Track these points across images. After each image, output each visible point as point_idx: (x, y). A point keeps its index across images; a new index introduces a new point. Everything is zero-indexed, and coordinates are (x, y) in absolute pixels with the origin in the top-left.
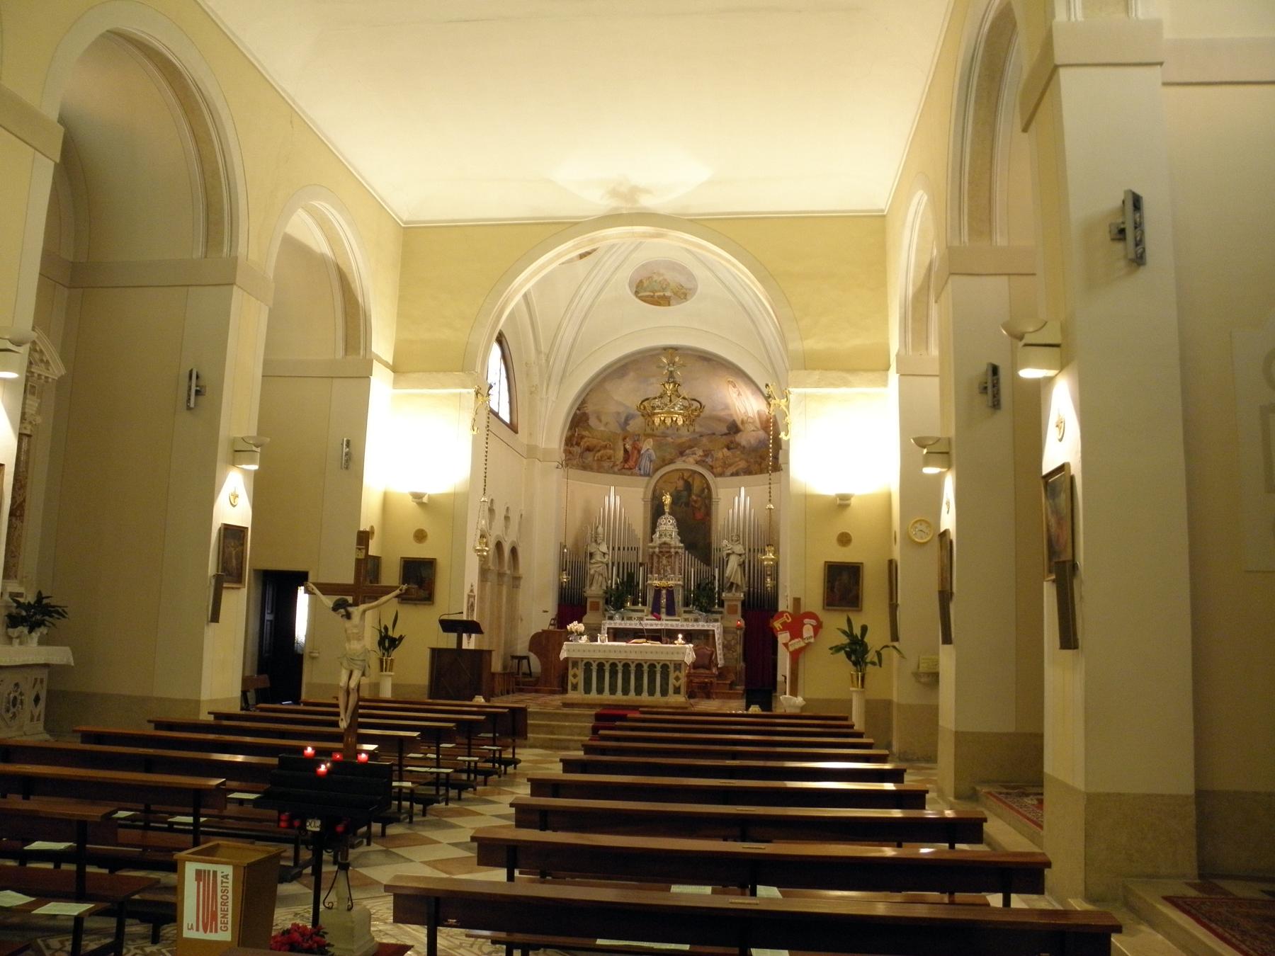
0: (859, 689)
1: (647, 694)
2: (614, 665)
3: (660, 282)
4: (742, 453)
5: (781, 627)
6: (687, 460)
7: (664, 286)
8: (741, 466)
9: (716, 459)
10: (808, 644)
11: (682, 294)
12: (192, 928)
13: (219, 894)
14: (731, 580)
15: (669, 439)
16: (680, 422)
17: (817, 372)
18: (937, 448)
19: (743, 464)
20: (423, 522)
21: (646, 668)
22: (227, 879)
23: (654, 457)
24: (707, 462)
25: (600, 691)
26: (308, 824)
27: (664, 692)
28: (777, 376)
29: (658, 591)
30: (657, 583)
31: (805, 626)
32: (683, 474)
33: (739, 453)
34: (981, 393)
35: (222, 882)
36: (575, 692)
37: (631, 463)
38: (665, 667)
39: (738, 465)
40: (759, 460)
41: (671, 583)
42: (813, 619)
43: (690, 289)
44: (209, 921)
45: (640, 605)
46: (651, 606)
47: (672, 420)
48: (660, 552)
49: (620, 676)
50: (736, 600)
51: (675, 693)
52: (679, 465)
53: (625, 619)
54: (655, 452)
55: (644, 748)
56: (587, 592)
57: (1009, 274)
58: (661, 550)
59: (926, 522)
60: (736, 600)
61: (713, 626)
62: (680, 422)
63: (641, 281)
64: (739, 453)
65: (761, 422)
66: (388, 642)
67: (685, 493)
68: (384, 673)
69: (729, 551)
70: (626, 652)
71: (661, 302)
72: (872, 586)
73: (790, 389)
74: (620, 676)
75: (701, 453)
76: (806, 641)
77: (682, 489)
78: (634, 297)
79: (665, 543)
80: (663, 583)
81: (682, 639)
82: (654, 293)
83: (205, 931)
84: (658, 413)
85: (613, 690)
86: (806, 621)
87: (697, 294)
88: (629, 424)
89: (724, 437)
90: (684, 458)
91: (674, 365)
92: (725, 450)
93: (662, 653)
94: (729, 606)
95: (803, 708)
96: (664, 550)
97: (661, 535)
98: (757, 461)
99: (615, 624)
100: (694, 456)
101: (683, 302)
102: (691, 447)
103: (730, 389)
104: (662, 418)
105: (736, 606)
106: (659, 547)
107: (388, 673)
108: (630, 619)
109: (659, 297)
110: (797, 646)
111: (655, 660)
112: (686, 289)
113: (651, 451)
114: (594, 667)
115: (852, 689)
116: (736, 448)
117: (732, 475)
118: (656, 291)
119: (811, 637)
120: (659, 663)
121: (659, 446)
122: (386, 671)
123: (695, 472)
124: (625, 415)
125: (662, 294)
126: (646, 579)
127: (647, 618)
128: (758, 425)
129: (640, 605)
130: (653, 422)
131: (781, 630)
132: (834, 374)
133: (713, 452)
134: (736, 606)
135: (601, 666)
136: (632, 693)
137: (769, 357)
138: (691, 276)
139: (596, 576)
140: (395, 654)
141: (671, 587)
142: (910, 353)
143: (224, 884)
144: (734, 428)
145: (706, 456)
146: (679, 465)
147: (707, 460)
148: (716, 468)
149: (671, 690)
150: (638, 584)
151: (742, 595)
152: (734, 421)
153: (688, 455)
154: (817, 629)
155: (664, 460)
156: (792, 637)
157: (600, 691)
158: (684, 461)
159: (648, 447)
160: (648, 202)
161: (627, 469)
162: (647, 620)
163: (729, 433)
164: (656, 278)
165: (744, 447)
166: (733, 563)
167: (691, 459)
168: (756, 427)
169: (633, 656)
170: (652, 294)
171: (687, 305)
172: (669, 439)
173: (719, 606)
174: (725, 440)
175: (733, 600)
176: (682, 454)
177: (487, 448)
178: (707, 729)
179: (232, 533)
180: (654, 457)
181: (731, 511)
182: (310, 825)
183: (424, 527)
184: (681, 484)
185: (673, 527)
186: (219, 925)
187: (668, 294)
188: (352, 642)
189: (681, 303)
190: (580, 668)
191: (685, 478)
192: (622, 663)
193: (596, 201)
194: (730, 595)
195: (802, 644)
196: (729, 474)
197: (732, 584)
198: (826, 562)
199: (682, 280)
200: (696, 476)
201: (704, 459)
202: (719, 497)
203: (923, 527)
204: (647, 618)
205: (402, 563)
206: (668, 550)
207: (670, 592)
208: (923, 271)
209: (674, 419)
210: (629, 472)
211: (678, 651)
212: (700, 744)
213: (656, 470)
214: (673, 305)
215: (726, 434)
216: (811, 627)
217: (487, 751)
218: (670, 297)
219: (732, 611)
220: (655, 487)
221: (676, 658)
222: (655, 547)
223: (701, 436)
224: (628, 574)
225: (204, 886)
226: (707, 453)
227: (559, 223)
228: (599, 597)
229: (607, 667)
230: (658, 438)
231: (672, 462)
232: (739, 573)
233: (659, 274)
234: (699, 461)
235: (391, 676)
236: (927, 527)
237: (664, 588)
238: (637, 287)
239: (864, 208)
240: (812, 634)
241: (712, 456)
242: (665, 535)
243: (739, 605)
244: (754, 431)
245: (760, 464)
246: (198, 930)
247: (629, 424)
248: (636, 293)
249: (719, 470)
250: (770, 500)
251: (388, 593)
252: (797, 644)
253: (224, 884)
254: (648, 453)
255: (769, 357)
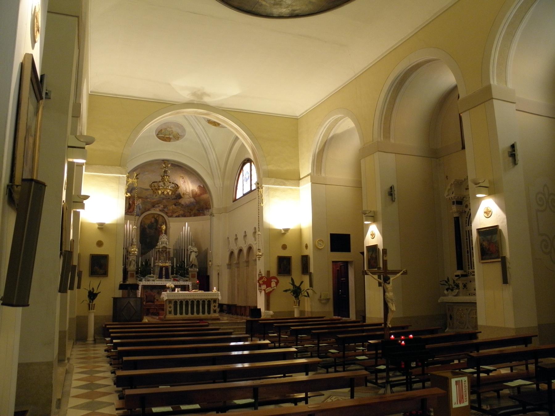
0: (298, 307)
1: (179, 314)
2: (204, 302)
3: (170, 131)
4: (181, 207)
5: (262, 283)
6: (156, 209)
7: (171, 133)
8: (181, 213)
9: (169, 210)
10: (273, 290)
11: (177, 137)
12: (456, 404)
13: (464, 388)
14: (193, 263)
15: (149, 200)
16: (170, 193)
17: (273, 179)
18: (370, 215)
19: (182, 212)
20: (100, 237)
21: (201, 302)
22: (466, 382)
23: (141, 207)
24: (165, 211)
25: (192, 313)
26: (412, 364)
27: (209, 312)
28: (213, 176)
29: (161, 268)
30: (161, 264)
31: (272, 283)
32: (154, 215)
33: (180, 207)
34: (389, 195)
35: (464, 383)
36: (171, 315)
37: (131, 210)
38: (209, 302)
39: (179, 213)
40: (190, 211)
41: (167, 264)
42: (275, 279)
43: (181, 136)
44: (461, 400)
45: (152, 274)
46: (158, 274)
47: (167, 192)
48: (162, 251)
49: (190, 306)
50: (195, 272)
51: (214, 313)
52: (152, 211)
53: (147, 281)
54: (142, 205)
55: (215, 338)
56: (129, 269)
57: (395, 153)
58: (163, 250)
59: (322, 241)
60: (195, 272)
61: (189, 283)
62: (170, 193)
63: (161, 130)
64: (180, 207)
65: (193, 195)
66: (92, 295)
67: (155, 224)
68: (91, 311)
69: (192, 251)
70: (193, 296)
71: (167, 140)
72: (296, 266)
73: (263, 185)
74: (190, 306)
75: (162, 206)
76: (273, 288)
77: (154, 222)
78: (156, 137)
79: (164, 247)
80: (164, 265)
81: (216, 289)
82: (165, 136)
83: (460, 404)
84: (161, 189)
85: (187, 313)
86: (273, 280)
87: (184, 138)
88: (132, 192)
89: (174, 200)
90: (154, 208)
91: (168, 168)
92: (174, 206)
93: (209, 295)
94: (192, 274)
95: (272, 316)
96: (164, 250)
97: (162, 243)
98: (189, 211)
99: (143, 283)
100: (159, 208)
101: (177, 141)
102: (158, 204)
103: (180, 179)
104: (163, 191)
105: (195, 274)
106: (162, 249)
107: (93, 311)
108: (149, 281)
109: (167, 138)
110: (269, 291)
111: (205, 299)
112: (180, 136)
113: (140, 205)
114: (178, 303)
115: (294, 307)
116: (179, 205)
117: (176, 217)
118: (166, 135)
119: (275, 287)
120: (201, 300)
121: (144, 203)
122: (91, 310)
123: (159, 215)
124: (131, 188)
125: (168, 136)
126: (154, 263)
127: (157, 280)
128: (191, 196)
129: (152, 274)
130: (158, 192)
131: (262, 284)
132: (280, 180)
133: (168, 206)
134: (195, 274)
135: (181, 302)
136: (195, 314)
137: (211, 168)
138: (184, 130)
139: (132, 261)
140: (95, 301)
141: (168, 266)
142: (315, 175)
143: (465, 384)
144: (179, 197)
145: (164, 208)
146: (152, 211)
147: (165, 210)
148: (169, 213)
149: (212, 311)
150: (150, 265)
151: (198, 270)
152: (180, 193)
153: (156, 207)
154: (277, 283)
155: (145, 209)
156: (267, 287)
157: (192, 313)
158: (154, 210)
159: (139, 203)
160: (207, 100)
161: (129, 212)
162: (157, 281)
163: (176, 199)
164: (168, 129)
165: (183, 205)
166: (193, 256)
167: (158, 209)
168: (190, 196)
169: (206, 297)
170: (164, 136)
171: (178, 143)
172: (149, 200)
173: (153, 274)
174: (174, 201)
175: (193, 272)
176: (153, 206)
177: (259, 209)
178: (195, 329)
179: (373, 249)
180: (141, 207)
181: (181, 233)
182: (412, 364)
183: (102, 239)
184: (153, 220)
185: (167, 239)
186: (464, 400)
187: (171, 137)
188: (390, 293)
189: (175, 141)
190: (172, 303)
191: (155, 217)
192: (191, 301)
193: (185, 96)
194: (192, 269)
195: (271, 290)
196: (175, 216)
197: (193, 264)
198: (278, 256)
199: (179, 131)
200: (160, 216)
201: (163, 209)
202: (170, 226)
203: (321, 243)
204: (157, 280)
205: (91, 257)
206: (165, 250)
207: (167, 268)
208: (323, 144)
209: (168, 192)
210: (130, 214)
211: (215, 294)
212: (132, 339)
213: (142, 213)
214: (172, 142)
215: (175, 199)
216: (275, 283)
217: (285, 338)
218: (171, 138)
219: (193, 276)
220: (142, 220)
221: (215, 297)
222: (159, 248)
223: (163, 199)
224: (146, 260)
225: (458, 386)
226: (165, 207)
227: (166, 103)
228: (134, 271)
229: (184, 303)
230: (143, 199)
231: (149, 210)
232: (196, 260)
233: (171, 128)
234: (161, 210)
235: (93, 312)
236: (322, 243)
237: (164, 266)
238: (159, 132)
239: (145, 97)
240: (275, 285)
241: (167, 208)
242: (164, 243)
243: (196, 273)
244: (188, 198)
245: (190, 213)
246: (458, 404)
247: (132, 192)
248: (157, 135)
249: (170, 214)
250: (259, 230)
251: (399, 273)
252: (269, 290)
253: (465, 384)
254: (139, 205)
255: (211, 168)
